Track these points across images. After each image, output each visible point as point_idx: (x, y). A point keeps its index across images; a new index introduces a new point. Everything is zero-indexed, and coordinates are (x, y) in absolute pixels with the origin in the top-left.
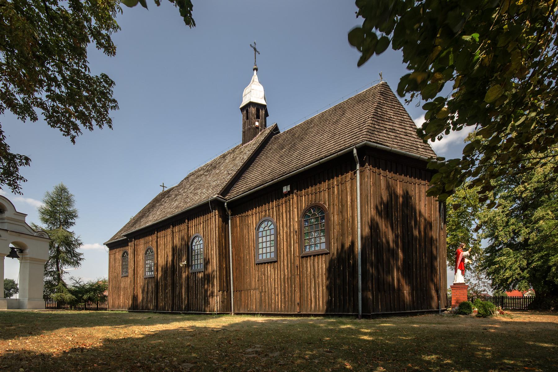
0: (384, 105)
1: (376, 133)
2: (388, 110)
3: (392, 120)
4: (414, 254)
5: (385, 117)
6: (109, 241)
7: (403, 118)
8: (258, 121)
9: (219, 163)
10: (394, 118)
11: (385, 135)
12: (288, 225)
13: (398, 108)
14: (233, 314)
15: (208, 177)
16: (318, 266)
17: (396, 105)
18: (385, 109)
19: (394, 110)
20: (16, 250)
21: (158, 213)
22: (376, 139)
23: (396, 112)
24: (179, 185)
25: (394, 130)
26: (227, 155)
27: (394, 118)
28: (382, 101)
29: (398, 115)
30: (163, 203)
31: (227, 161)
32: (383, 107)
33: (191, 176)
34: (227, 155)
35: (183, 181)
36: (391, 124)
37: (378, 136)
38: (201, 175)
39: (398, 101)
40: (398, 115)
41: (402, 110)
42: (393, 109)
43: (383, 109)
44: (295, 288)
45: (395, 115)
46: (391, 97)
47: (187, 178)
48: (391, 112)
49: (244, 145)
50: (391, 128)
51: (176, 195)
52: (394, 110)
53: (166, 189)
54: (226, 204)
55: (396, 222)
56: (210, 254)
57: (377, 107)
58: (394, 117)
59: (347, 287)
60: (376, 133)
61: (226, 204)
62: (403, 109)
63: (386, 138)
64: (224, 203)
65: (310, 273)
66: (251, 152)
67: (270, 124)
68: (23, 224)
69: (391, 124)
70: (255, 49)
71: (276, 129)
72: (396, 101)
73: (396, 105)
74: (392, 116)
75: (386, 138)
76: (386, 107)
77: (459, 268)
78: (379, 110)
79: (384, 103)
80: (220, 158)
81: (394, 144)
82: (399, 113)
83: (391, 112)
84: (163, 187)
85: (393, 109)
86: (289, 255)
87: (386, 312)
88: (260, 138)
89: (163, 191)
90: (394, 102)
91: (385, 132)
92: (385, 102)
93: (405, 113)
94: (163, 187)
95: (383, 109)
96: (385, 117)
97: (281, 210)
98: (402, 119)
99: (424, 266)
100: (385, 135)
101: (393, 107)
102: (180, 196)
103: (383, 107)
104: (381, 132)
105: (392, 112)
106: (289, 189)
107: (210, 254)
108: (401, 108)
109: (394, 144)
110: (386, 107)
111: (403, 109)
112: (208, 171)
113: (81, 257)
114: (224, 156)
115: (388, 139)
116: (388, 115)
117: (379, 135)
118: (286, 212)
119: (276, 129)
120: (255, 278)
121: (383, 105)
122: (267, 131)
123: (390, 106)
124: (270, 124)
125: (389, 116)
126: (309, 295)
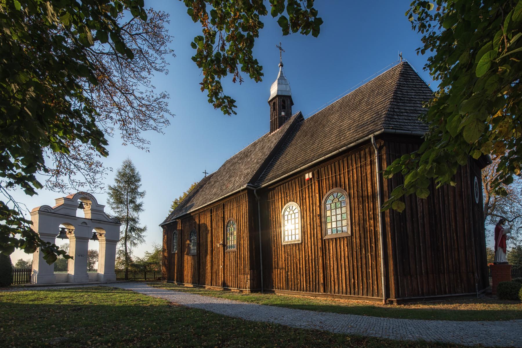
0: (404, 86)
1: (396, 117)
2: (408, 91)
3: (413, 101)
4: (443, 235)
5: (406, 99)
6: (163, 223)
7: (425, 96)
8: (284, 111)
9: (251, 151)
10: (415, 98)
11: (406, 118)
12: (311, 209)
13: (420, 86)
14: (262, 290)
15: (241, 165)
16: (340, 248)
17: (417, 84)
18: (405, 91)
19: (415, 89)
20: (97, 234)
21: (200, 199)
22: (396, 123)
23: (418, 91)
24: (218, 172)
25: (416, 110)
26: (257, 143)
27: (415, 98)
28: (401, 83)
29: (420, 94)
30: (205, 189)
31: (257, 149)
32: (404, 88)
33: (227, 163)
34: (257, 143)
35: (220, 168)
36: (412, 105)
37: (398, 120)
38: (235, 163)
39: (419, 79)
40: (420, 94)
41: (424, 87)
42: (414, 89)
43: (403, 91)
44: (318, 269)
45: (416, 94)
46: (412, 76)
47: (224, 165)
48: (412, 92)
49: (272, 134)
50: (413, 108)
51: (215, 182)
52: (415, 89)
53: (207, 175)
54: (255, 191)
55: (421, 204)
56: (242, 236)
57: (397, 90)
58: (416, 97)
59: (370, 270)
60: (396, 117)
61: (255, 191)
62: (426, 87)
63: (406, 121)
64: (253, 190)
65: (333, 255)
66: (278, 140)
67: (295, 113)
68: (102, 214)
69: (412, 105)
70: (280, 48)
71: (300, 116)
72: (418, 80)
73: (417, 84)
74: (413, 96)
75: (406, 121)
76: (406, 88)
77: (499, 246)
78: (399, 92)
79: (404, 84)
80: (252, 145)
81: (415, 126)
82: (421, 92)
83: (412, 92)
84: (206, 173)
85: (414, 89)
86: (312, 238)
87: (413, 296)
88: (286, 126)
89: (205, 177)
90: (415, 81)
91: (406, 114)
92: (405, 83)
93: (428, 90)
94: (206, 173)
95: (403, 91)
96: (406, 99)
97: (304, 196)
98: (425, 97)
99: (456, 247)
100: (406, 118)
101: (414, 86)
102: (218, 183)
103: (404, 88)
104: (401, 115)
105: (413, 91)
106: (311, 176)
107: (242, 236)
108: (423, 86)
109: (415, 126)
110: (406, 88)
111: (426, 87)
112: (241, 159)
113: (262, 77)
114: (255, 145)
115: (408, 121)
116: (408, 96)
117: (399, 119)
118: (309, 197)
119: (300, 116)
120: (282, 258)
121: (403, 86)
122: (292, 120)
123: (411, 86)
124: (295, 113)
125: (410, 97)
126: (333, 276)
